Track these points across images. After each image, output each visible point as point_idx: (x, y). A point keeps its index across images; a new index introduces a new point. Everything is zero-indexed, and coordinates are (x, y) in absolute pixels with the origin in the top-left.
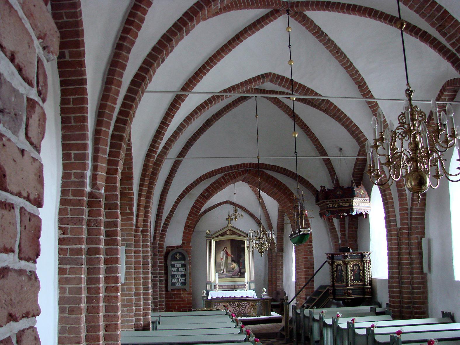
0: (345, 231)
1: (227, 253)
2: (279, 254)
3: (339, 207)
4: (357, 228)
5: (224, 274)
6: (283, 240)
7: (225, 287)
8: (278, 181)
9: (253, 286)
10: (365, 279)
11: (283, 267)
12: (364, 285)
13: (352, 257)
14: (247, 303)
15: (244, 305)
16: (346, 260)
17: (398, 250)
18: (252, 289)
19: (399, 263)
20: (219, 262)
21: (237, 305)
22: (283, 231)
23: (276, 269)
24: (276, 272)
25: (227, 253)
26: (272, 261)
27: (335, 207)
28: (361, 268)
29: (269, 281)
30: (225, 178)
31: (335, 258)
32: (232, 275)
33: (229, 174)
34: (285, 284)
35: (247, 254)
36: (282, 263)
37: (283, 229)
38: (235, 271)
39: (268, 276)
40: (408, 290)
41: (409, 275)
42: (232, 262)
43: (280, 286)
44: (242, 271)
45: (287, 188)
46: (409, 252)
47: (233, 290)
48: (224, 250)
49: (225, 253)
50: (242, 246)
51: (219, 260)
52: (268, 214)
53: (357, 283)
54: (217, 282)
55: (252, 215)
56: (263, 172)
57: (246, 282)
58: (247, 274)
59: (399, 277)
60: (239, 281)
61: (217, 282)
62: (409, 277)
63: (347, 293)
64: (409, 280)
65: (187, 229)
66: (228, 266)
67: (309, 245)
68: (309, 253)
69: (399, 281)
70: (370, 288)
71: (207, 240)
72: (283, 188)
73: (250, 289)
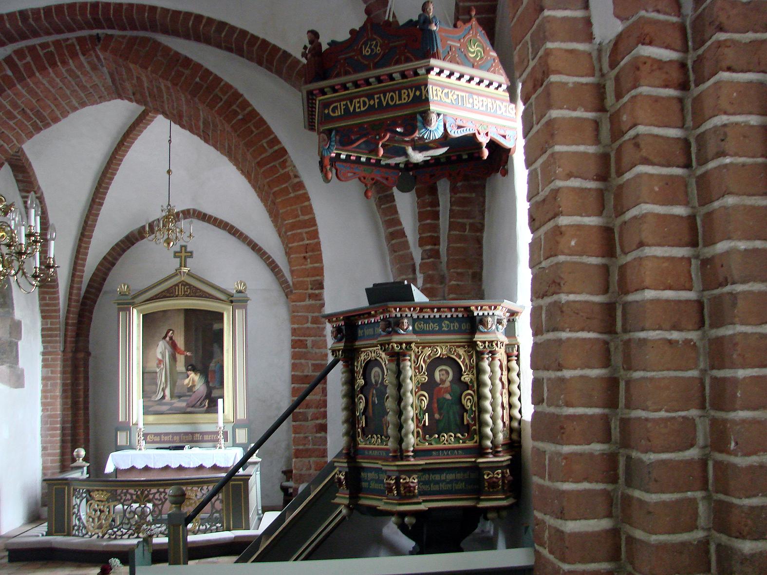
0: (436, 241)
1: (173, 345)
3: (371, 110)
4: (479, 228)
5: (166, 404)
7: (166, 438)
8: (208, 72)
9: (242, 435)
10: (482, 424)
12: (481, 451)
13: (422, 325)
15: (157, 496)
16: (396, 338)
17: (600, 214)
19: (609, 309)
21: (134, 497)
25: (173, 345)
27: (355, 115)
28: (466, 378)
30: (19, 63)
31: (360, 332)
32: (188, 406)
33: (32, 49)
35: (228, 350)
40: (685, 537)
41: (693, 413)
42: (187, 370)
45: (237, 95)
46: (692, 218)
47: (182, 448)
48: (168, 338)
49: (168, 346)
50: (216, 326)
51: (152, 365)
53: (448, 440)
54: (141, 425)
55: (255, 247)
56: (157, 44)
59: (606, 419)
60: (204, 422)
62: (689, 423)
63: (398, 489)
64: (693, 453)
67: (311, 296)
68: (309, 325)
69: (611, 459)
70: (508, 466)
71: (120, 310)
72: (225, 98)
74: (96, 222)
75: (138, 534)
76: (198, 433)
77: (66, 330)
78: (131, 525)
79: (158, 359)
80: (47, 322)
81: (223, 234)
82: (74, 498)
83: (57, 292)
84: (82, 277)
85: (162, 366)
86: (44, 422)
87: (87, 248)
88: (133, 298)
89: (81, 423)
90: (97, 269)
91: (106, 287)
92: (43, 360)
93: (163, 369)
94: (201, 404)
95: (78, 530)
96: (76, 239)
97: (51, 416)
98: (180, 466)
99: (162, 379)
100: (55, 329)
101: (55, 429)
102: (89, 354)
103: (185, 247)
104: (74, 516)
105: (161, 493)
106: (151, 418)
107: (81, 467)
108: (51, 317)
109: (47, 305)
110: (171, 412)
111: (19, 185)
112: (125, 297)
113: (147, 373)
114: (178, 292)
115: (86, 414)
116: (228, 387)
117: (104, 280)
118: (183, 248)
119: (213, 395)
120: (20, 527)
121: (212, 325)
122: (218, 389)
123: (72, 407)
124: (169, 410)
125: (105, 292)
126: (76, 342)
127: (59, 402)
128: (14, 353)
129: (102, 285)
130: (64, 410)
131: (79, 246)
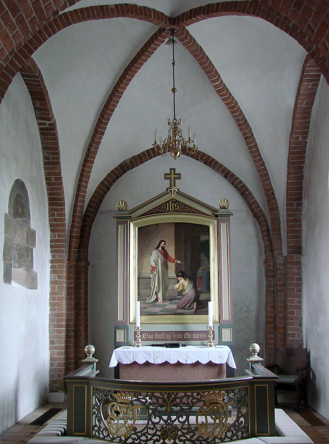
1: (165, 254)
2: (292, 258)
5: (158, 306)
6: (300, 226)
7: (159, 336)
9: (227, 335)
11: (300, 291)
14: (195, 395)
15: (185, 400)
20: (147, 275)
21: (160, 401)
22: (300, 205)
23: (286, 296)
24: (285, 302)
25: (165, 254)
26: (274, 276)
29: (267, 323)
32: (178, 308)
34: (307, 331)
35: (214, 258)
36: (300, 279)
37: (300, 199)
44: (202, 297)
47: (177, 346)
48: (160, 249)
49: (160, 255)
50: (203, 238)
51: (147, 272)
52: (263, 164)
54: (138, 324)
55: (227, 175)
57: (211, 324)
58: (213, 306)
61: (138, 324)
65: (51, 178)
71: (118, 223)
73: (221, 343)
74: (98, 149)
75: (164, 440)
77: (70, 242)
78: (157, 430)
79: (152, 266)
80: (55, 235)
81: (199, 164)
82: (94, 397)
83: (63, 209)
84: (84, 196)
85: (155, 273)
86: (51, 320)
87: (90, 172)
88: (130, 213)
89: (82, 322)
90: (96, 192)
91: (103, 207)
92: (52, 267)
93: (156, 274)
94: (190, 306)
95: (98, 431)
96: (80, 164)
97: (58, 315)
98: (178, 362)
99: (155, 284)
100: (62, 241)
101: (61, 326)
102: (88, 263)
103: (174, 169)
104: (94, 416)
105: (188, 397)
106: (145, 318)
107: (92, 363)
108: (57, 231)
109: (56, 220)
110: (162, 313)
111: (37, 113)
112: (123, 212)
113: (141, 278)
114: (169, 208)
115: (86, 315)
116: (214, 291)
117: (101, 201)
118: (173, 171)
119: (200, 299)
120: (34, 411)
121: (199, 237)
122: (204, 293)
123: (75, 308)
124: (161, 311)
125: (101, 213)
126: (79, 252)
127: (64, 303)
128: (30, 257)
129: (99, 206)
130: (68, 310)
131: (83, 170)
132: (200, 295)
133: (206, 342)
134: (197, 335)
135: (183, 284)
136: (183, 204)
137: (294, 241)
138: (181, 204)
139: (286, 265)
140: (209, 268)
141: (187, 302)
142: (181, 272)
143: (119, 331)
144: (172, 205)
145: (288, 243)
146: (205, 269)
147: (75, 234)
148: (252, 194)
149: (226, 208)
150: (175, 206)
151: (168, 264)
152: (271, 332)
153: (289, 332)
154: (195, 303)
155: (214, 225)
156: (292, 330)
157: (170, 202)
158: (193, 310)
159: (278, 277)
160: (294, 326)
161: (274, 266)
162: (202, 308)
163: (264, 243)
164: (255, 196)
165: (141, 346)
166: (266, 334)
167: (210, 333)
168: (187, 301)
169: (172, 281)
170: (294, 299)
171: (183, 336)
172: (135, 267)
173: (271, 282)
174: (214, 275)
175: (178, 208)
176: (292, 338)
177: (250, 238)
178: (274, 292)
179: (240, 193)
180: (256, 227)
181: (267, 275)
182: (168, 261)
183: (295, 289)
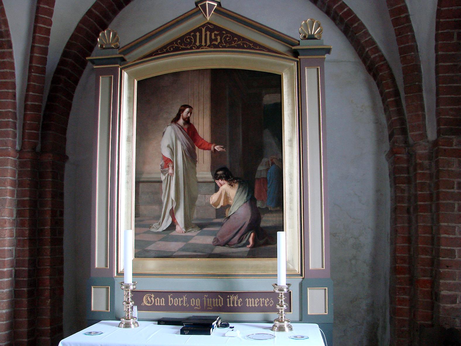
5: (176, 239)
7: (177, 302)
18: (312, 320)
20: (154, 176)
29: (395, 270)
32: (217, 243)
35: (291, 141)
38: (227, 225)
39: (394, 251)
43: (454, 302)
44: (267, 221)
48: (181, 122)
49: (181, 135)
50: (268, 99)
57: (282, 281)
66: (196, 198)
76: (235, 294)
79: (164, 157)
85: (170, 171)
93: (172, 174)
94: (240, 240)
113: (143, 182)
119: (262, 224)
122: (271, 212)
130: (18, 243)
132: (262, 216)
133: (273, 316)
134: (254, 301)
135: (226, 193)
136: (228, 32)
137: (451, 110)
138: (224, 32)
139: (437, 157)
140: (281, 161)
141: (235, 231)
142: (224, 169)
143: (97, 289)
144: (206, 35)
145: (438, 114)
146: (273, 163)
147: (31, 101)
148: (364, 26)
149: (316, 39)
150: (213, 37)
151: (197, 152)
152: (404, 289)
153: (444, 293)
154: (252, 235)
155: (290, 68)
156: (450, 288)
157: (204, 30)
158: (247, 249)
159: (418, 181)
160: (455, 280)
161: (408, 161)
162: (266, 243)
163: (389, 118)
164: (370, 32)
165: (132, 326)
166: (393, 291)
167: (280, 300)
168: (234, 229)
169: (204, 188)
170: (454, 225)
171: (225, 302)
172: (129, 158)
173: (403, 191)
174: (291, 175)
175: (219, 40)
176: (449, 305)
177: (361, 111)
178: (408, 212)
179: (342, 28)
180: (371, 92)
181: (395, 178)
182: (197, 148)
183: (456, 206)
